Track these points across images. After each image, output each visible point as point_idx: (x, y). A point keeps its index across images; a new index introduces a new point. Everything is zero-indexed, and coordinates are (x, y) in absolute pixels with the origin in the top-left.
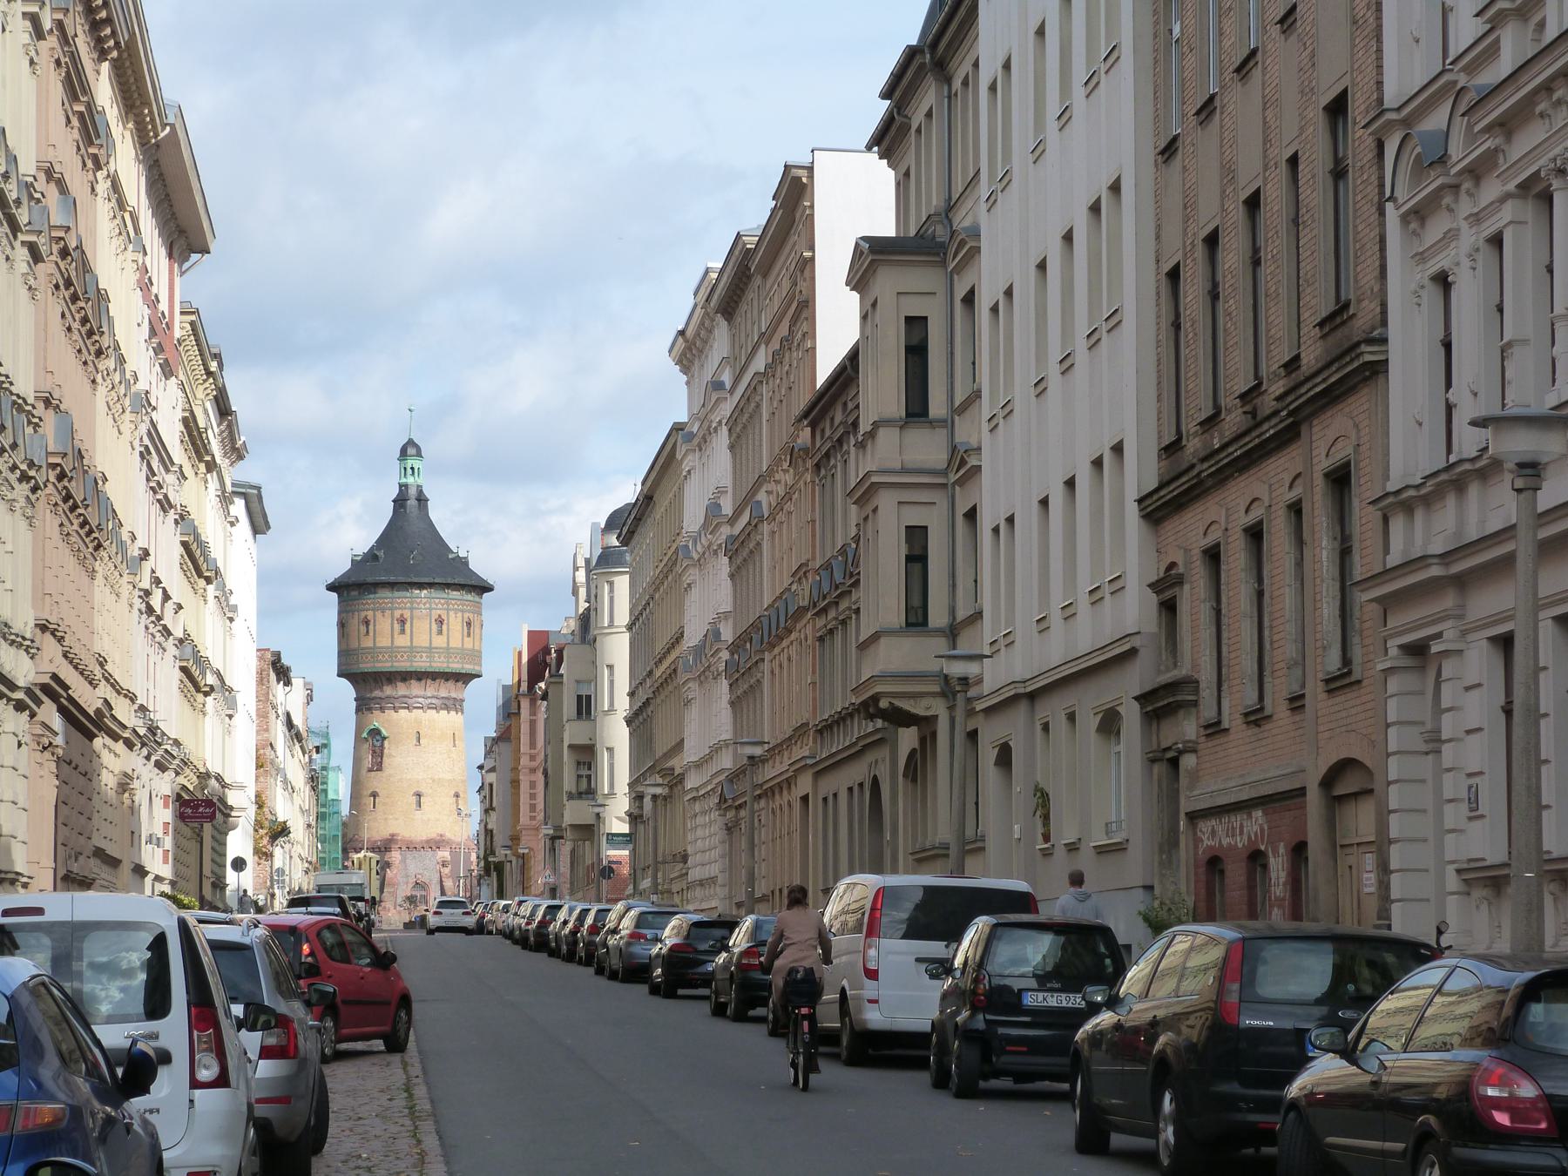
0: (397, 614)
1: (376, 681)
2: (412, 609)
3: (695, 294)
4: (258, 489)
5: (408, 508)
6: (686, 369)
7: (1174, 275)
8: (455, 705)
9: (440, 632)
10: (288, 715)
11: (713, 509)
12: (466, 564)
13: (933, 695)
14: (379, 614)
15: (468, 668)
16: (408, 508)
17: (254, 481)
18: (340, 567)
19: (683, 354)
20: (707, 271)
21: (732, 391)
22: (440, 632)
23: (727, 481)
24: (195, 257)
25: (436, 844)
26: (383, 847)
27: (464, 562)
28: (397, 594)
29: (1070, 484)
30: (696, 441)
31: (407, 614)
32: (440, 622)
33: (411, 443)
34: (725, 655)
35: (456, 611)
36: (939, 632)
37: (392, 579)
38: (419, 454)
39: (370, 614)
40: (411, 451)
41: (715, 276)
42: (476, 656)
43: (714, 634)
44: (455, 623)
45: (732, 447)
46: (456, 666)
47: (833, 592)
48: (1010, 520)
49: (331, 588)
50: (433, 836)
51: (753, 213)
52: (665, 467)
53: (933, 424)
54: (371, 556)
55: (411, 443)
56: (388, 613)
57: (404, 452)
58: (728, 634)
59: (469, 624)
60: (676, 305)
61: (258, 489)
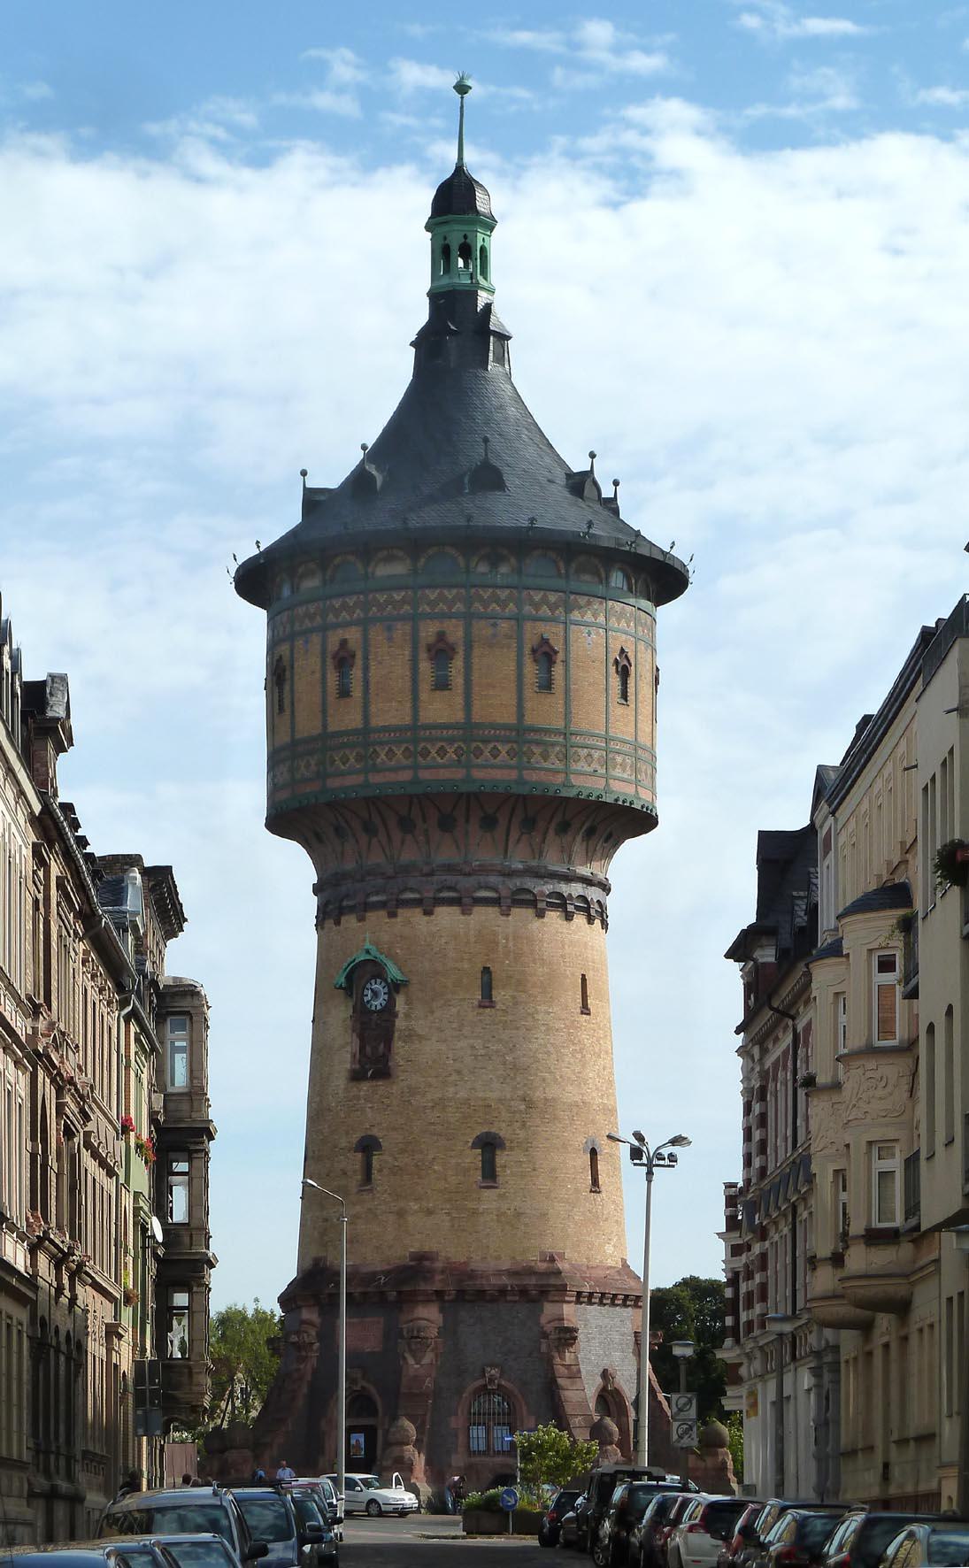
0: (428, 631)
22: (442, 685)
31: (455, 632)
56: (402, 629)
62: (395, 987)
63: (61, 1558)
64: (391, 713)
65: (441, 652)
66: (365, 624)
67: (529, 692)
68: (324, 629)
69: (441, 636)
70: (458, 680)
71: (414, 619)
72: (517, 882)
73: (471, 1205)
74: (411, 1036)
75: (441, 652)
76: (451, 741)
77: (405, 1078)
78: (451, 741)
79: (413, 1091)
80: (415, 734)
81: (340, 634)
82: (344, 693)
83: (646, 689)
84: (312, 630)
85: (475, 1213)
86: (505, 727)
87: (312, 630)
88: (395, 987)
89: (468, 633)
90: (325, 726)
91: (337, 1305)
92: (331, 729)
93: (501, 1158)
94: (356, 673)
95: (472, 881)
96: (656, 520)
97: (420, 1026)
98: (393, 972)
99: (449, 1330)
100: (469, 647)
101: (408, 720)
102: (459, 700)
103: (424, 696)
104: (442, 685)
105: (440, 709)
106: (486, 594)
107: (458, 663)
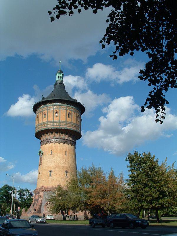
0: (44, 112)
67: (43, 118)
68: (42, 111)
69: (57, 111)
72: (56, 140)
73: (48, 179)
76: (45, 124)
78: (45, 124)
79: (43, 166)
81: (44, 111)
84: (41, 111)
85: (48, 180)
86: (65, 121)
87: (41, 111)
89: (48, 111)
90: (60, 120)
91: (13, 201)
92: (48, 121)
93: (52, 173)
94: (46, 115)
95: (50, 140)
97: (44, 159)
100: (48, 113)
101: (46, 121)
102: (46, 119)
103: (43, 119)
106: (50, 107)
107: (71, 115)
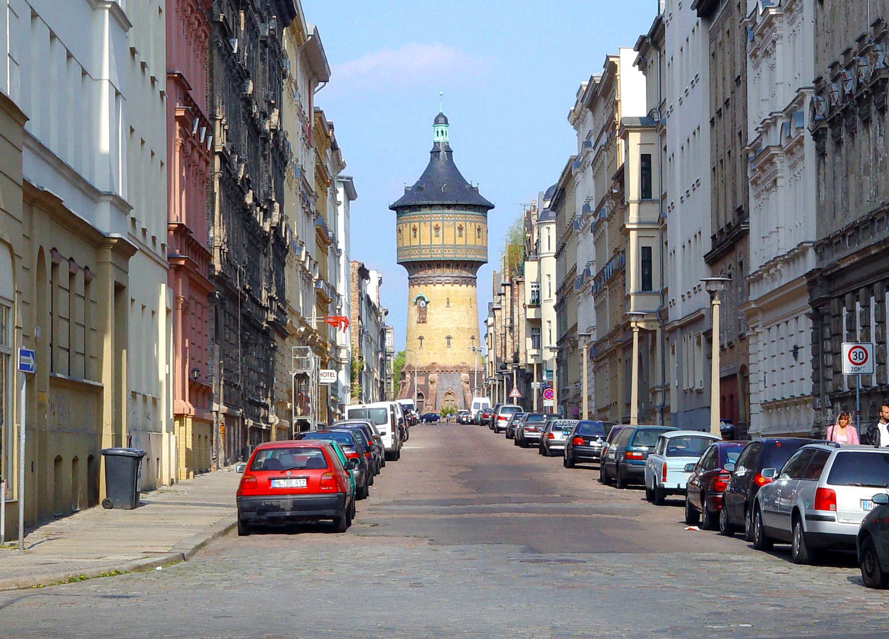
0: (434, 224)
1: (420, 266)
2: (443, 221)
3: (578, 94)
4: (351, 179)
5: (441, 155)
6: (576, 128)
7: (714, 169)
8: (472, 281)
9: (460, 236)
10: (368, 296)
11: (586, 207)
12: (477, 191)
13: (654, 321)
14: (422, 224)
15: (479, 258)
16: (441, 155)
17: (349, 175)
18: (397, 195)
19: (575, 121)
20: (581, 87)
21: (594, 148)
22: (460, 236)
23: (592, 194)
24: (321, 84)
25: (458, 369)
26: (424, 372)
27: (475, 191)
28: (433, 212)
29: (690, 242)
30: (581, 167)
31: (440, 225)
32: (461, 229)
33: (441, 115)
34: (592, 283)
35: (471, 222)
36: (656, 293)
37: (431, 202)
38: (446, 122)
39: (417, 224)
40: (442, 120)
41: (585, 88)
42: (484, 250)
43: (587, 272)
44: (470, 230)
45: (594, 177)
46: (471, 257)
47: (611, 277)
48: (700, 233)
49: (392, 208)
50: (459, 363)
51: (599, 72)
52: (568, 177)
53: (653, 202)
54: (418, 187)
55: (441, 115)
56: (428, 223)
57: (437, 122)
58: (593, 272)
59: (479, 230)
60: (570, 102)
61: (351, 179)
62: (427, 303)
63: (102, 48)
64: (426, 242)
65: (437, 229)
66: (466, 221)
70: (464, 235)
71: (431, 221)
74: (431, 314)
75: (437, 229)
77: (429, 323)
80: (431, 247)
82: (415, 236)
83: (484, 234)
88: (427, 303)
96: (486, 194)
97: (433, 311)
98: (427, 300)
99: (440, 380)
104: (437, 236)
105: (437, 241)
107: (441, 231)
